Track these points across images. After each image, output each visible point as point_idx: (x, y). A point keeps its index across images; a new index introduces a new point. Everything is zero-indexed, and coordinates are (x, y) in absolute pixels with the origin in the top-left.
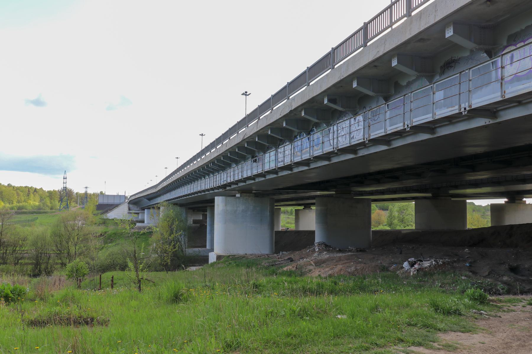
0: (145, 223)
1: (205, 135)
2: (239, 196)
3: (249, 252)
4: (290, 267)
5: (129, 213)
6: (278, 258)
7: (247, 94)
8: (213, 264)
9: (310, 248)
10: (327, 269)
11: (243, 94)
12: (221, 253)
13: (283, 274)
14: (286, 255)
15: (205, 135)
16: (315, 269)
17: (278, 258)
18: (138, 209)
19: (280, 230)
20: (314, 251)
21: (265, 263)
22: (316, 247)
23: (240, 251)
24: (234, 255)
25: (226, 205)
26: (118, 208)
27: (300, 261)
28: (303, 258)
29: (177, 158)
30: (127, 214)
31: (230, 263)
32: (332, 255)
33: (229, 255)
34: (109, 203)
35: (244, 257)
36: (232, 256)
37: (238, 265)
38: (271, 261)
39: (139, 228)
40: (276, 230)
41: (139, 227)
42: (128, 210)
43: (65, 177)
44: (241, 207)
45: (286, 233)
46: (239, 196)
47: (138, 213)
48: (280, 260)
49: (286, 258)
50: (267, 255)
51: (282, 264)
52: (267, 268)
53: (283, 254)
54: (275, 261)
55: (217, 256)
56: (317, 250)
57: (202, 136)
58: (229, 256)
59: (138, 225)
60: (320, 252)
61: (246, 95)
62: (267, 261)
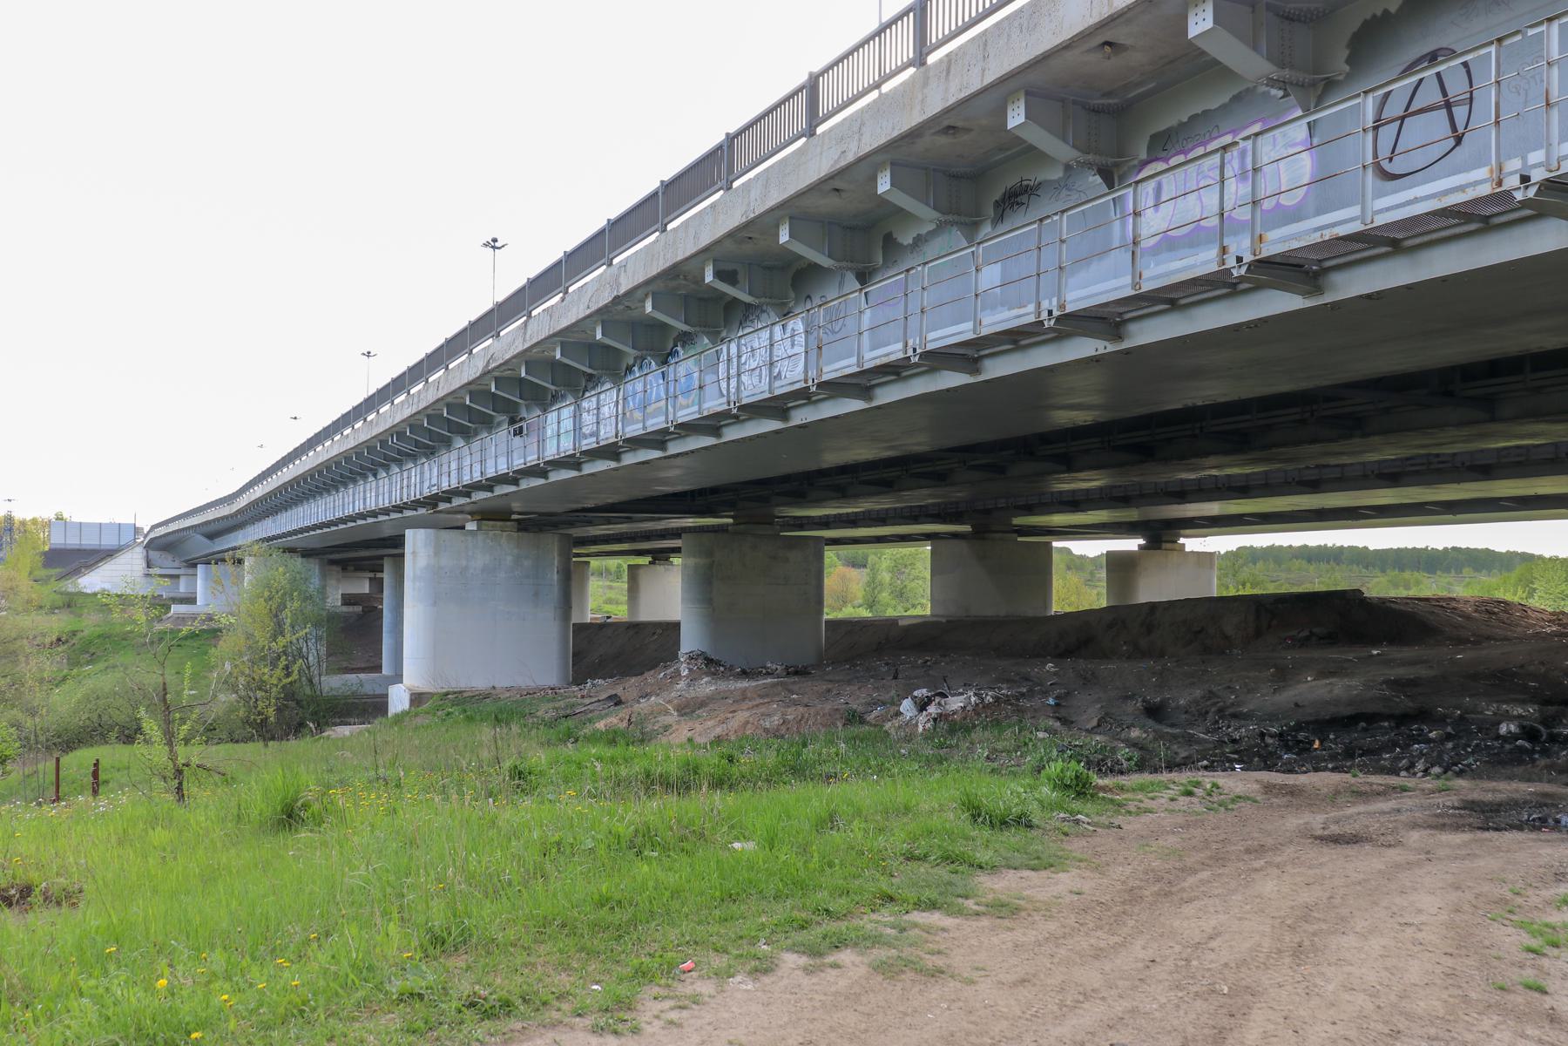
0: (198, 603)
2: (475, 528)
3: (502, 682)
4: (614, 720)
5: (148, 575)
7: (497, 244)
12: (423, 686)
13: (594, 739)
14: (602, 687)
17: (583, 697)
18: (176, 564)
21: (545, 711)
24: (461, 692)
25: (436, 554)
26: (113, 562)
27: (639, 702)
28: (646, 695)
31: (448, 714)
32: (723, 685)
33: (444, 691)
34: (84, 547)
38: (562, 704)
42: (144, 565)
45: (603, 628)
48: (587, 701)
49: (604, 696)
52: (550, 724)
53: (594, 685)
55: (412, 695)
58: (447, 694)
59: (176, 609)
62: (551, 705)
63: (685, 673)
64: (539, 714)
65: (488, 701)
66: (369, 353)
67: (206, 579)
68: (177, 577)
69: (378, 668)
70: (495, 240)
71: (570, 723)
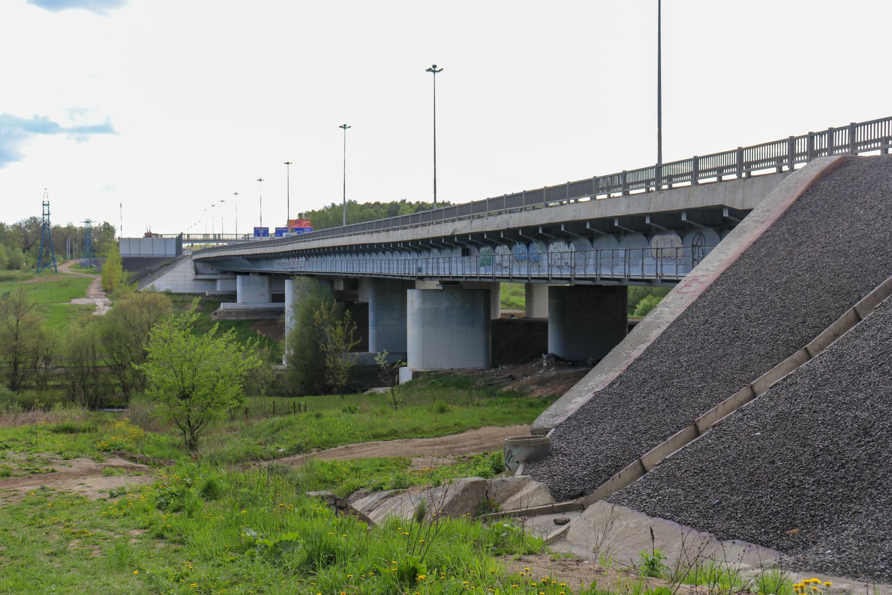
0: (238, 302)
1: (350, 127)
2: (442, 288)
3: (456, 366)
4: (510, 387)
5: (195, 280)
6: (497, 375)
7: (436, 69)
8: (408, 384)
9: (537, 361)
10: (550, 389)
11: (429, 70)
12: (419, 368)
13: (501, 395)
14: (505, 370)
15: (350, 127)
16: (537, 389)
17: (497, 375)
18: (214, 271)
19: (500, 317)
20: (541, 366)
21: (480, 382)
22: (545, 361)
23: (444, 365)
24: (437, 371)
25: (423, 302)
26: (173, 270)
27: (523, 379)
28: (526, 376)
29: (288, 163)
30: (193, 282)
31: (433, 383)
32: (560, 372)
33: (429, 370)
34: (142, 256)
35: (450, 374)
36: (434, 372)
37: (445, 386)
38: (487, 379)
39: (227, 312)
40: (492, 318)
41: (228, 311)
42: (194, 272)
43: (46, 203)
44: (445, 304)
45: (506, 323)
46: (442, 288)
47: (215, 280)
48: (499, 378)
49: (507, 375)
50: (482, 371)
51: (501, 383)
52: (485, 387)
53: (502, 369)
54: (493, 380)
55: (413, 373)
56: (545, 364)
57: (345, 128)
58: (430, 372)
59: (223, 306)
60: (548, 367)
61: (434, 72)
62: (483, 379)
63: (545, 364)
64: (477, 383)
65: (451, 376)
66: (345, 125)
67: (243, 285)
68: (215, 280)
69: (366, 348)
70: (435, 66)
71: (492, 388)
